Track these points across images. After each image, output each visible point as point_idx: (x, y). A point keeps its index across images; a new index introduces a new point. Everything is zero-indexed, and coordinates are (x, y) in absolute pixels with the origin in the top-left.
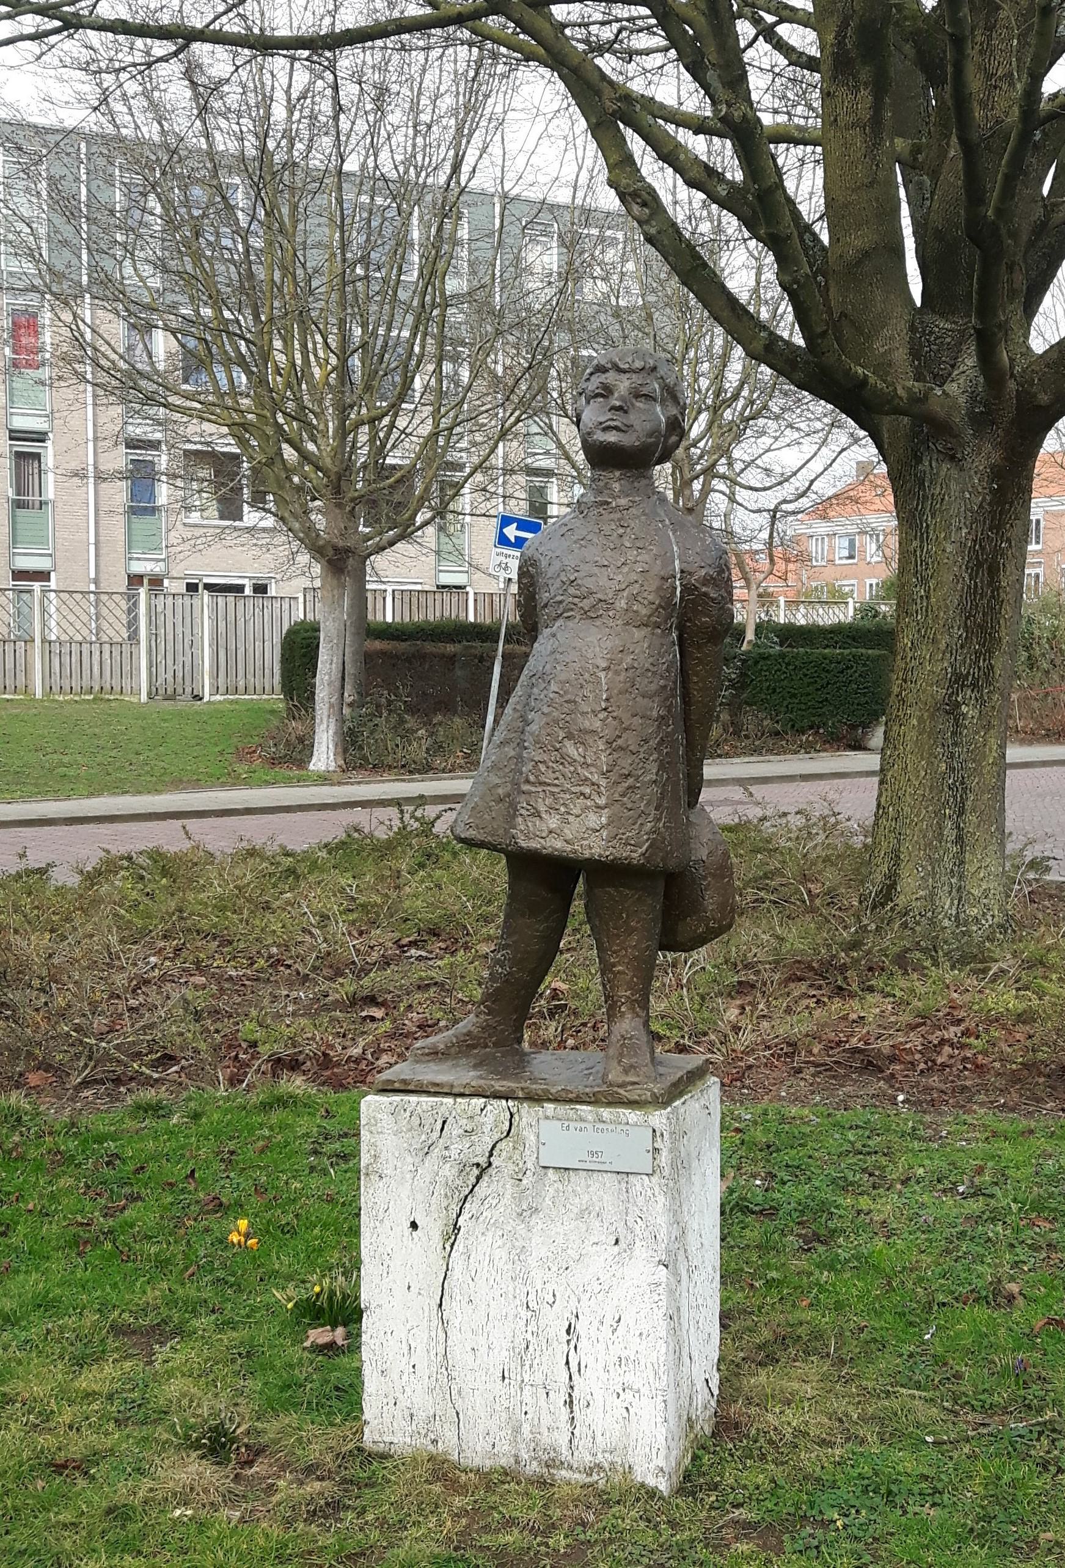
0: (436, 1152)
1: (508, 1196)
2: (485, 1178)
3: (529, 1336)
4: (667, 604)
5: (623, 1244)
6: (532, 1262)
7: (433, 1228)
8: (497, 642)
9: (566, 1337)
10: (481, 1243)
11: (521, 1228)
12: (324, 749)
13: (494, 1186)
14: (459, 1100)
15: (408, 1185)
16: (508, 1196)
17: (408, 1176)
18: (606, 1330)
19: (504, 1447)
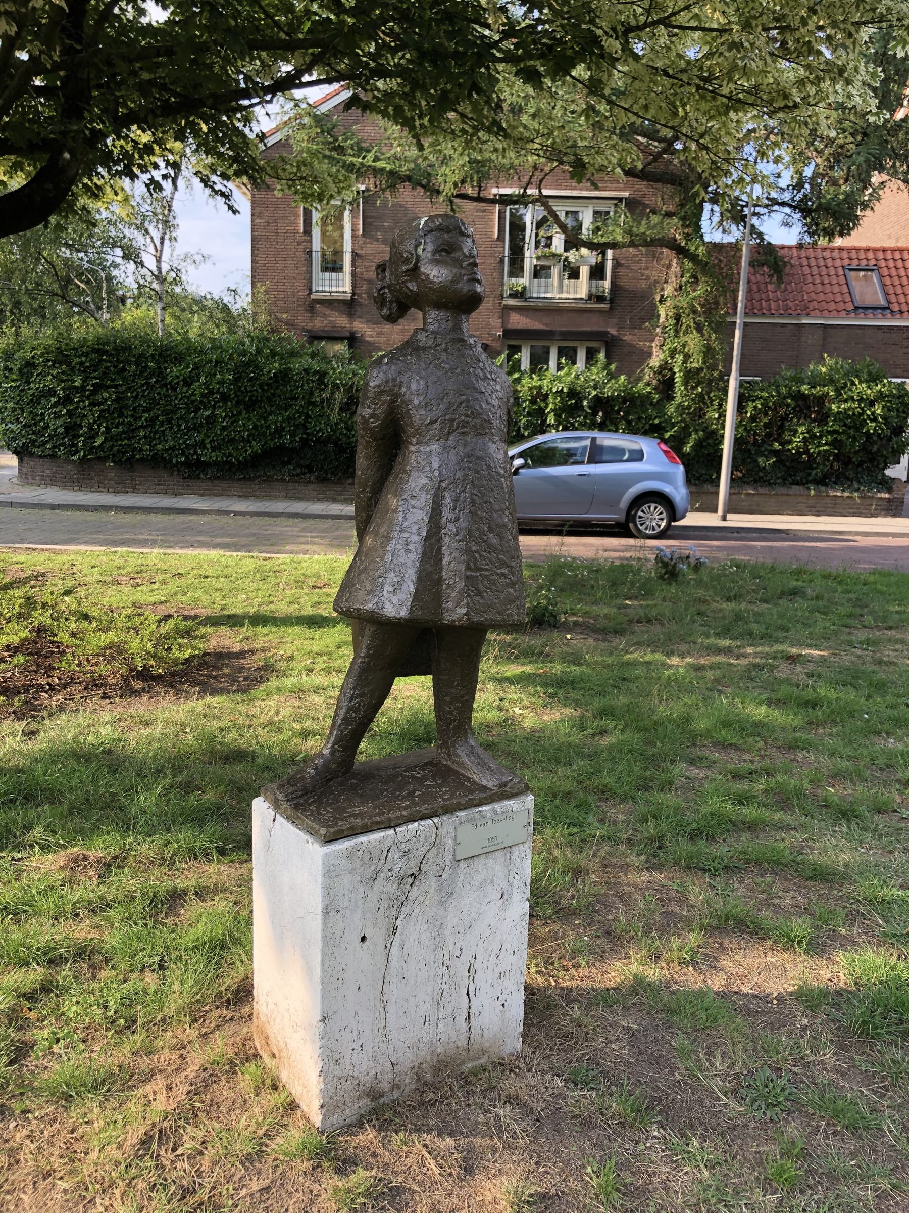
0: (382, 876)
1: (432, 891)
2: (417, 883)
3: (444, 986)
4: (354, 333)
5: (505, 897)
6: (447, 932)
7: (376, 936)
8: (738, 442)
9: (467, 974)
10: (415, 931)
11: (441, 911)
12: (41, 557)
13: (422, 888)
14: (398, 829)
15: (360, 911)
16: (432, 891)
17: (360, 902)
18: (493, 958)
19: (454, 1038)
